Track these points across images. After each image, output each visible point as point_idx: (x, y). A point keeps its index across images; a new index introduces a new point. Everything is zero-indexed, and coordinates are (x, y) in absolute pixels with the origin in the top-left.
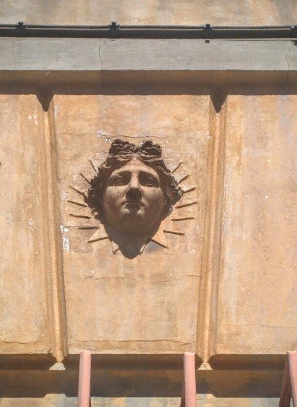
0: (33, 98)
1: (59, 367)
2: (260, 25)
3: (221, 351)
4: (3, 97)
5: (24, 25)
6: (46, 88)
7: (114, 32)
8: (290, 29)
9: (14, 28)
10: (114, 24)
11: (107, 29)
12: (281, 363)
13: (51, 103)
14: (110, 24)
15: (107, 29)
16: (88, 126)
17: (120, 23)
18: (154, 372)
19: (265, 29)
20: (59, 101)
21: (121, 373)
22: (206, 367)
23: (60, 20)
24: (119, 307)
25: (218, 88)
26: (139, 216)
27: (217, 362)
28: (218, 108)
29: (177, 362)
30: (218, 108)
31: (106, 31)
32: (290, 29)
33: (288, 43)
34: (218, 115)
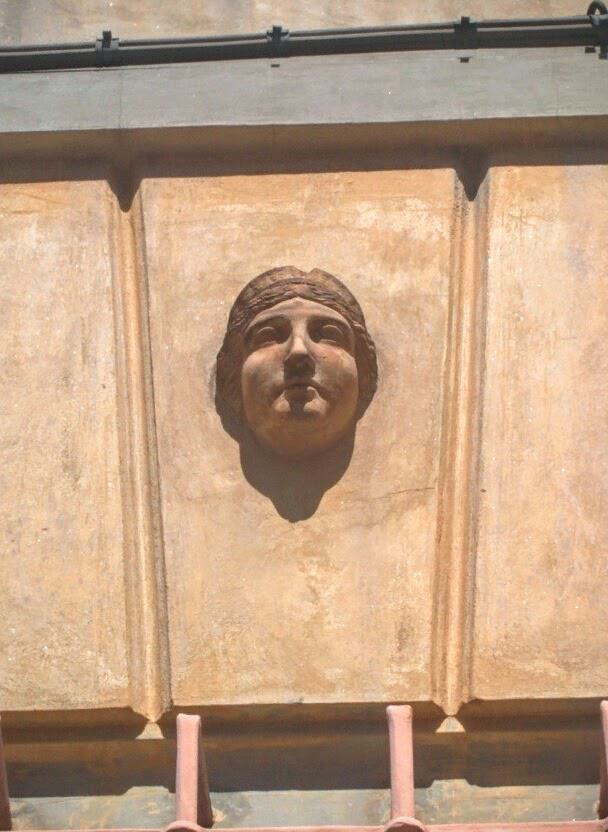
0: (102, 187)
1: (152, 732)
2: (17, 44)
3: (486, 693)
4: (2, 186)
5: (471, 22)
6: (124, 163)
7: (107, 56)
8: (589, 25)
9: (452, 31)
10: (465, 20)
11: (264, 41)
12: (584, 713)
13: (482, 186)
14: (271, 29)
15: (264, 41)
16: (215, 236)
17: (289, 26)
18: (327, 745)
19: (53, 52)
20: (158, 194)
21: (268, 746)
22: (451, 726)
23: (46, 32)
24: (326, 607)
25: (471, 153)
26: (313, 414)
27: (475, 714)
28: (471, 193)
29: (372, 720)
30: (471, 193)
31: (262, 44)
32: (93, 50)
33: (575, 56)
34: (471, 205)
